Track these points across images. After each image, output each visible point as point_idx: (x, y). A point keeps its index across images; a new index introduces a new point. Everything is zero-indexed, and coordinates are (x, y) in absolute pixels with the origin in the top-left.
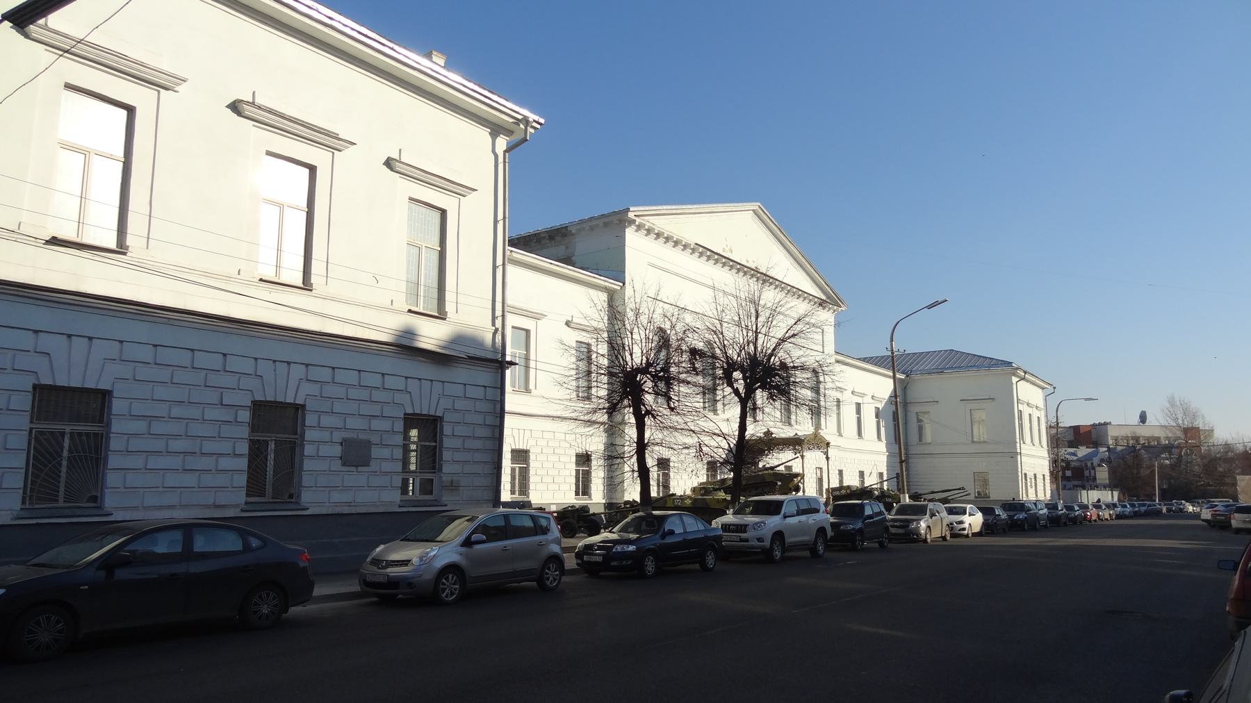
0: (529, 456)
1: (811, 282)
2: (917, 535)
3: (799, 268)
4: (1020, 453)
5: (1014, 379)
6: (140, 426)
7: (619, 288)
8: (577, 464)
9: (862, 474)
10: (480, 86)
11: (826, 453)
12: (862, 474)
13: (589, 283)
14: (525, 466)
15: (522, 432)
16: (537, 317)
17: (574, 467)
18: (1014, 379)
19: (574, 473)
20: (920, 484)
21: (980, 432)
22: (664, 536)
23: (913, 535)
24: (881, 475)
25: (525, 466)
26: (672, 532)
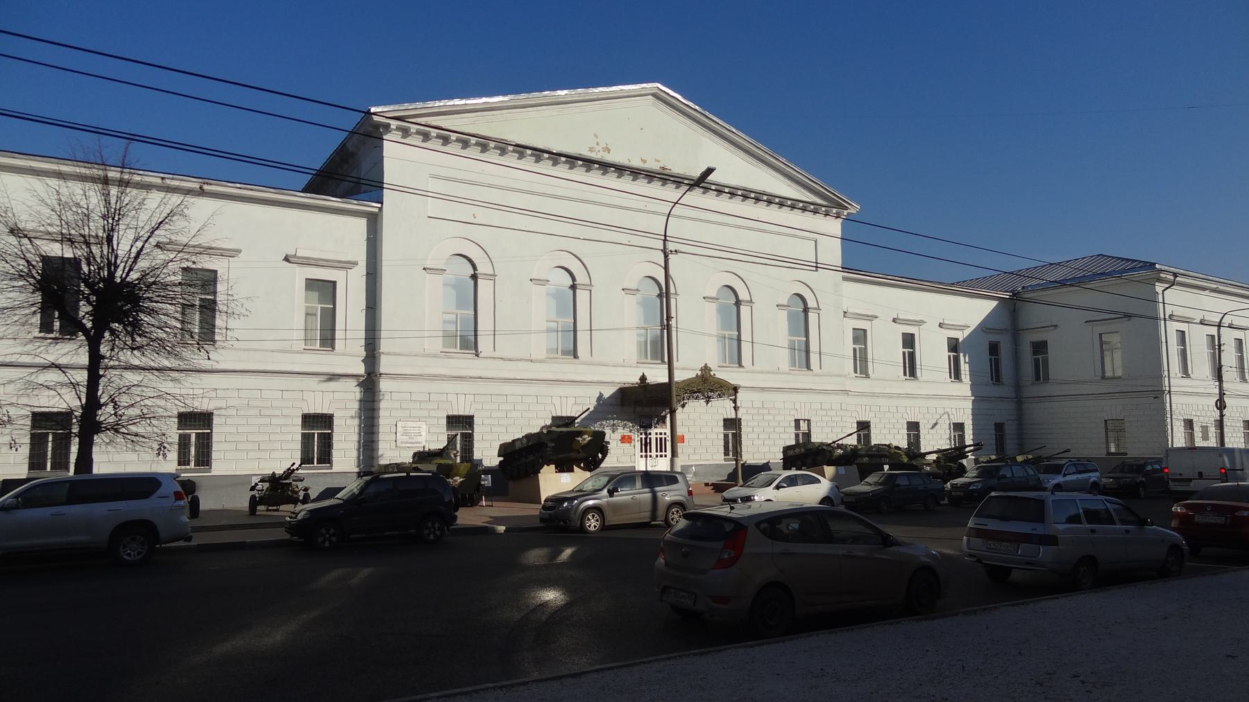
0: (212, 419)
1: (789, 182)
2: (565, 522)
3: (761, 165)
4: (1169, 392)
5: (1159, 288)
6: (433, 413)
7: (377, 210)
8: (908, 429)
9: (913, 427)
10: (685, 97)
11: (735, 401)
12: (913, 427)
13: (316, 207)
14: (209, 431)
15: (958, 409)
16: (919, 323)
17: (905, 431)
18: (1159, 288)
19: (722, 436)
20: (1043, 431)
21: (1115, 364)
22: (999, 478)
23: (559, 521)
24: (959, 427)
25: (209, 431)
26: (1004, 477)
